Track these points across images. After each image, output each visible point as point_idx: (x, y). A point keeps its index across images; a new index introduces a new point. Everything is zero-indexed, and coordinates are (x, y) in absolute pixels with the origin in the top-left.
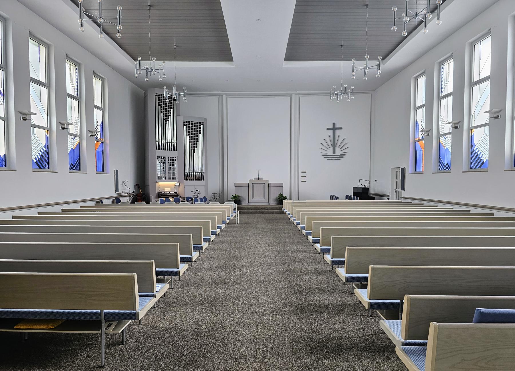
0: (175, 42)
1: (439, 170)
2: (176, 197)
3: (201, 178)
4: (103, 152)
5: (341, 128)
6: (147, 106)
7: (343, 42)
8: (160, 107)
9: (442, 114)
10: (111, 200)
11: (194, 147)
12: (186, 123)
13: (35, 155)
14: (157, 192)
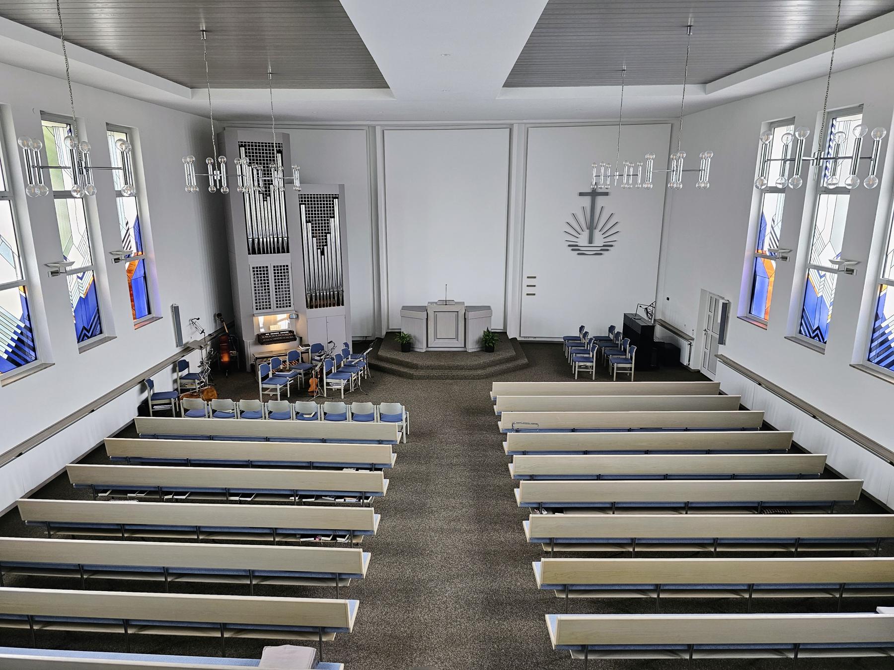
1: (800, 332)
4: (145, 277)
8: (315, 239)
9: (820, 223)
14: (256, 334)
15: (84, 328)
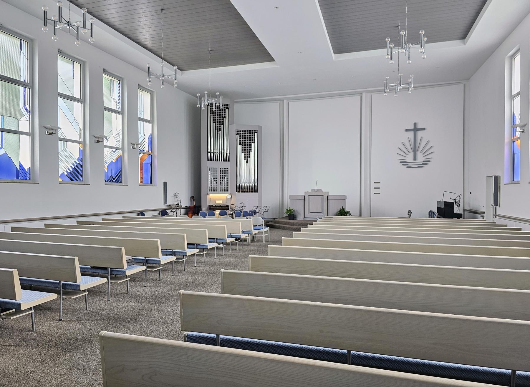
0: (210, 47)
2: (224, 209)
3: (254, 189)
4: (151, 164)
5: (424, 129)
6: (208, 115)
7: (399, 21)
8: (212, 116)
10: (158, 212)
11: (247, 157)
12: (238, 132)
13: (65, 166)
15: (112, 176)
